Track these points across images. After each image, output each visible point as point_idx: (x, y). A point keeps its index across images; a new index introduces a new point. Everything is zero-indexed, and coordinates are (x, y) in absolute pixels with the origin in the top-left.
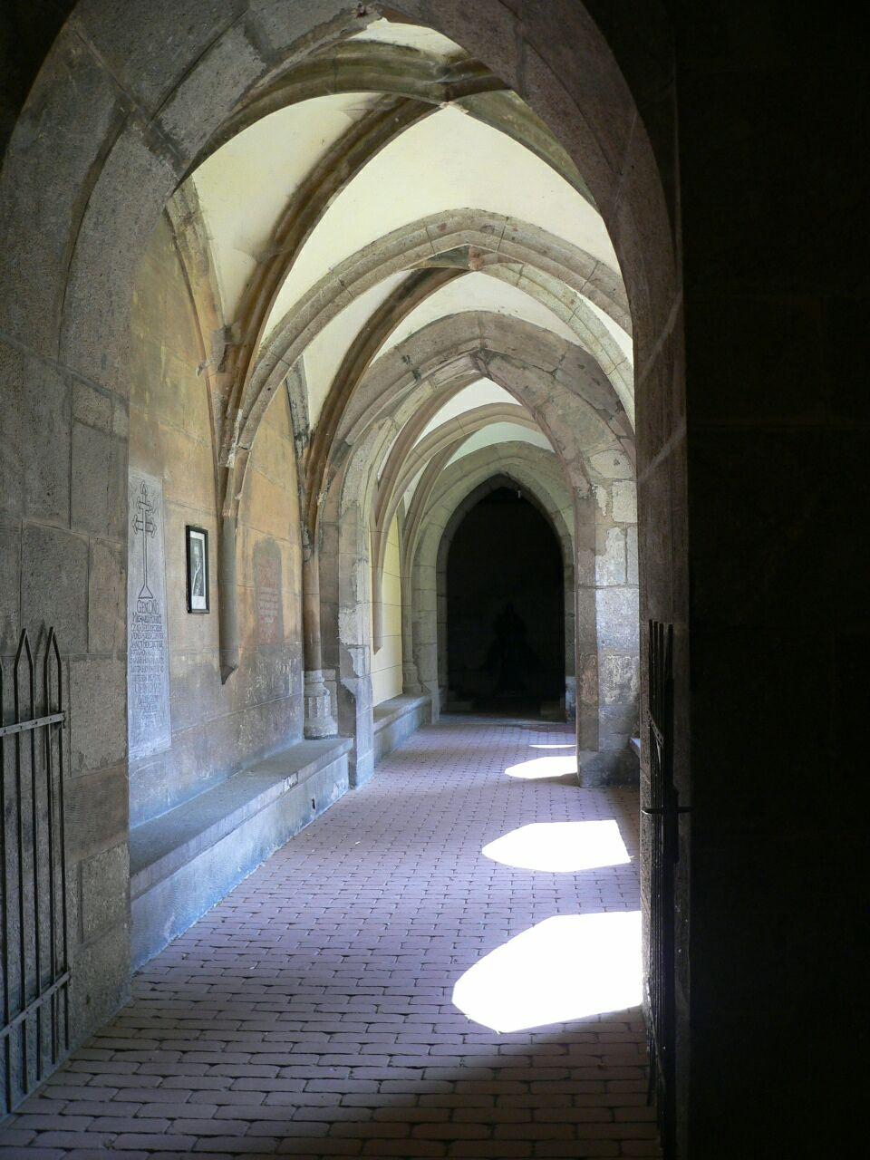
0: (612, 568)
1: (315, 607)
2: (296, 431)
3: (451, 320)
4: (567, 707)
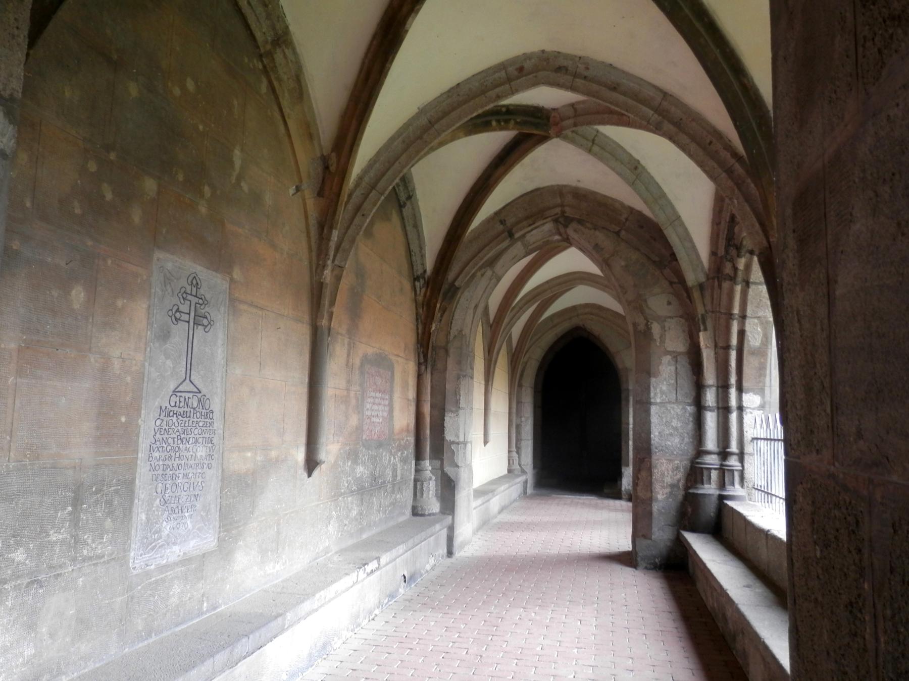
0: (664, 388)
1: (427, 409)
2: (415, 274)
4: (623, 489)
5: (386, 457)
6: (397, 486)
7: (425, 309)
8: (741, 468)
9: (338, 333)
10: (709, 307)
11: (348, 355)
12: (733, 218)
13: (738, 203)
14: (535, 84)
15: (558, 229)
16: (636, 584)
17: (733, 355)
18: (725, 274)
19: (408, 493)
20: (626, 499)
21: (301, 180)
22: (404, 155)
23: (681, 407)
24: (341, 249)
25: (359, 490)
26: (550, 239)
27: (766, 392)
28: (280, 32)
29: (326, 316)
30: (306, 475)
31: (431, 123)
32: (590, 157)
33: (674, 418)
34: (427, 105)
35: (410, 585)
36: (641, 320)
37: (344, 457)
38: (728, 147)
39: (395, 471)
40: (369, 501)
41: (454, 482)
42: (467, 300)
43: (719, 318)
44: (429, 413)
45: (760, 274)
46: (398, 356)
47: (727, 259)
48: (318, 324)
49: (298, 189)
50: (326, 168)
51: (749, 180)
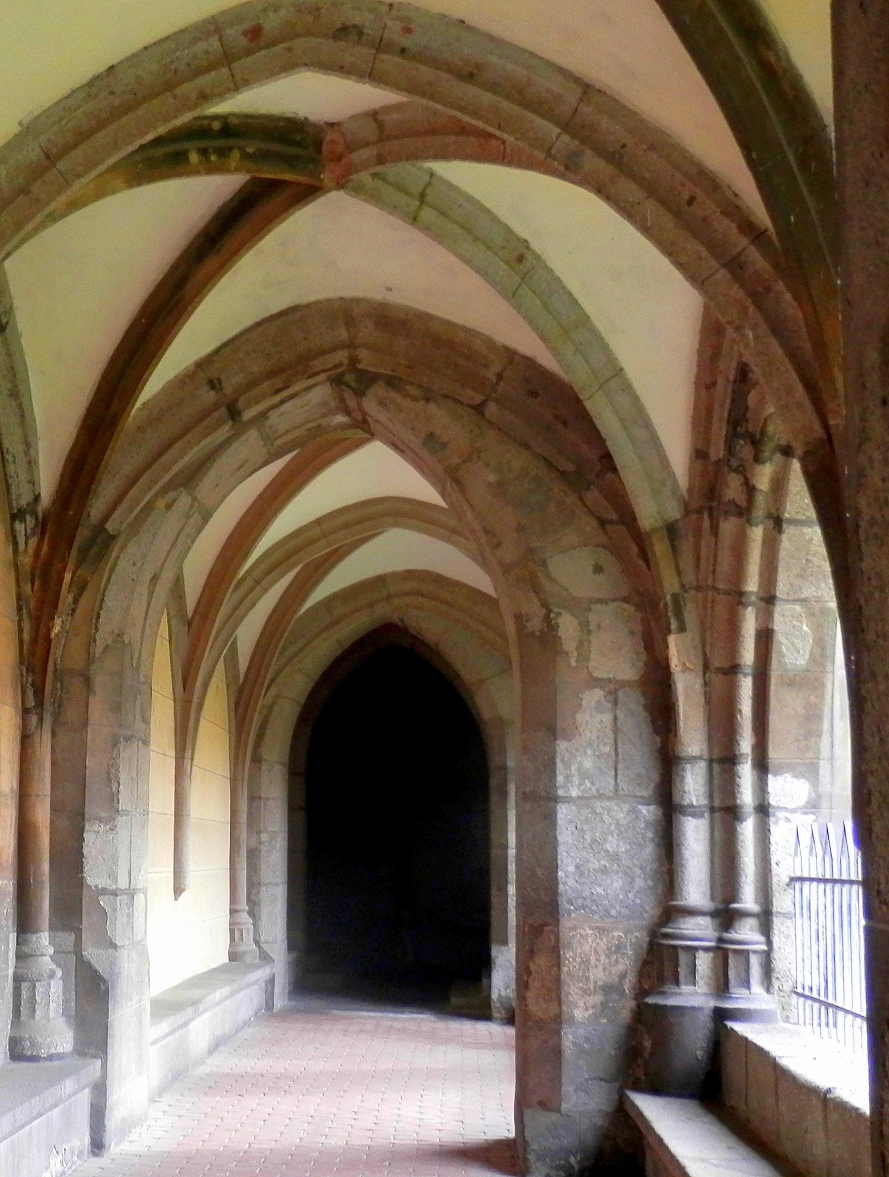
0: (588, 764)
1: (42, 814)
2: (14, 504)
3: (296, 316)
4: (494, 996)
7: (36, 584)
8: (765, 948)
10: (689, 578)
12: (743, 372)
13: (756, 337)
15: (342, 400)
17: (746, 687)
20: (501, 1019)
23: (626, 807)
26: (324, 421)
34: (38, 117)
36: (533, 608)
41: (104, 981)
45: (807, 500)
47: (729, 467)
51: (780, 286)
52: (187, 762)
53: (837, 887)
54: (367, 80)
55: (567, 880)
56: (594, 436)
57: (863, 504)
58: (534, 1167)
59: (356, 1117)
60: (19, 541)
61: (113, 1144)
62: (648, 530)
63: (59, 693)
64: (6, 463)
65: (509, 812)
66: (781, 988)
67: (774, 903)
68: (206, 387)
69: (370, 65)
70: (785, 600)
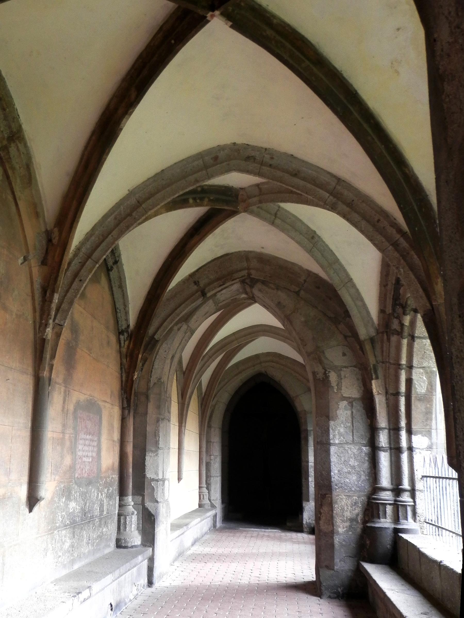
0: (342, 430)
1: (130, 449)
2: (120, 329)
4: (304, 522)
5: (94, 493)
6: (103, 521)
7: (128, 359)
8: (413, 504)
9: (56, 383)
10: (380, 359)
11: (64, 402)
12: (398, 281)
13: (404, 271)
14: (228, 170)
15: (245, 289)
16: (321, 612)
17: (402, 400)
18: (393, 329)
19: (113, 527)
20: (307, 532)
21: (28, 251)
22: (117, 229)
23: (357, 447)
24: (61, 310)
25: (71, 524)
26: (237, 297)
27: (432, 434)
28: (15, 130)
29: (47, 368)
30: (27, 510)
31: (139, 203)
32: (273, 228)
33: (352, 458)
34: (136, 188)
35: (116, 613)
36: (320, 370)
37: (60, 494)
38: (394, 224)
39: (101, 506)
40: (80, 534)
41: (153, 516)
42: (165, 351)
43: (389, 367)
44: (132, 453)
45: (424, 329)
46: (105, 402)
47: (394, 316)
48: (41, 375)
49: (25, 259)
50: (49, 241)
51: (412, 253)
52: (183, 428)
53: (441, 480)
54: (257, 176)
55: (335, 476)
56: (342, 304)
57: (453, 350)
58: (324, 592)
59: (252, 572)
60: (122, 343)
61: (156, 582)
62: (363, 340)
63: (136, 402)
64: (117, 313)
65: (309, 448)
66: (420, 520)
67: (416, 486)
68: (193, 284)
69: (258, 170)
70: (417, 367)
